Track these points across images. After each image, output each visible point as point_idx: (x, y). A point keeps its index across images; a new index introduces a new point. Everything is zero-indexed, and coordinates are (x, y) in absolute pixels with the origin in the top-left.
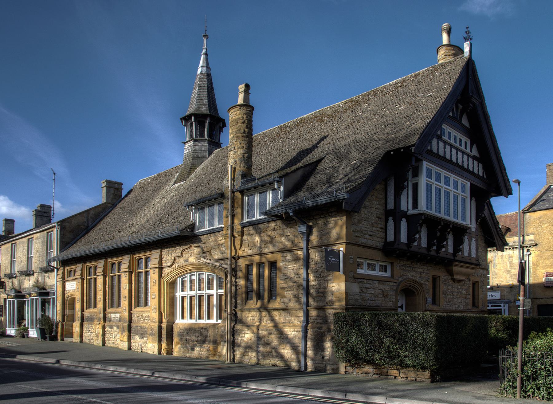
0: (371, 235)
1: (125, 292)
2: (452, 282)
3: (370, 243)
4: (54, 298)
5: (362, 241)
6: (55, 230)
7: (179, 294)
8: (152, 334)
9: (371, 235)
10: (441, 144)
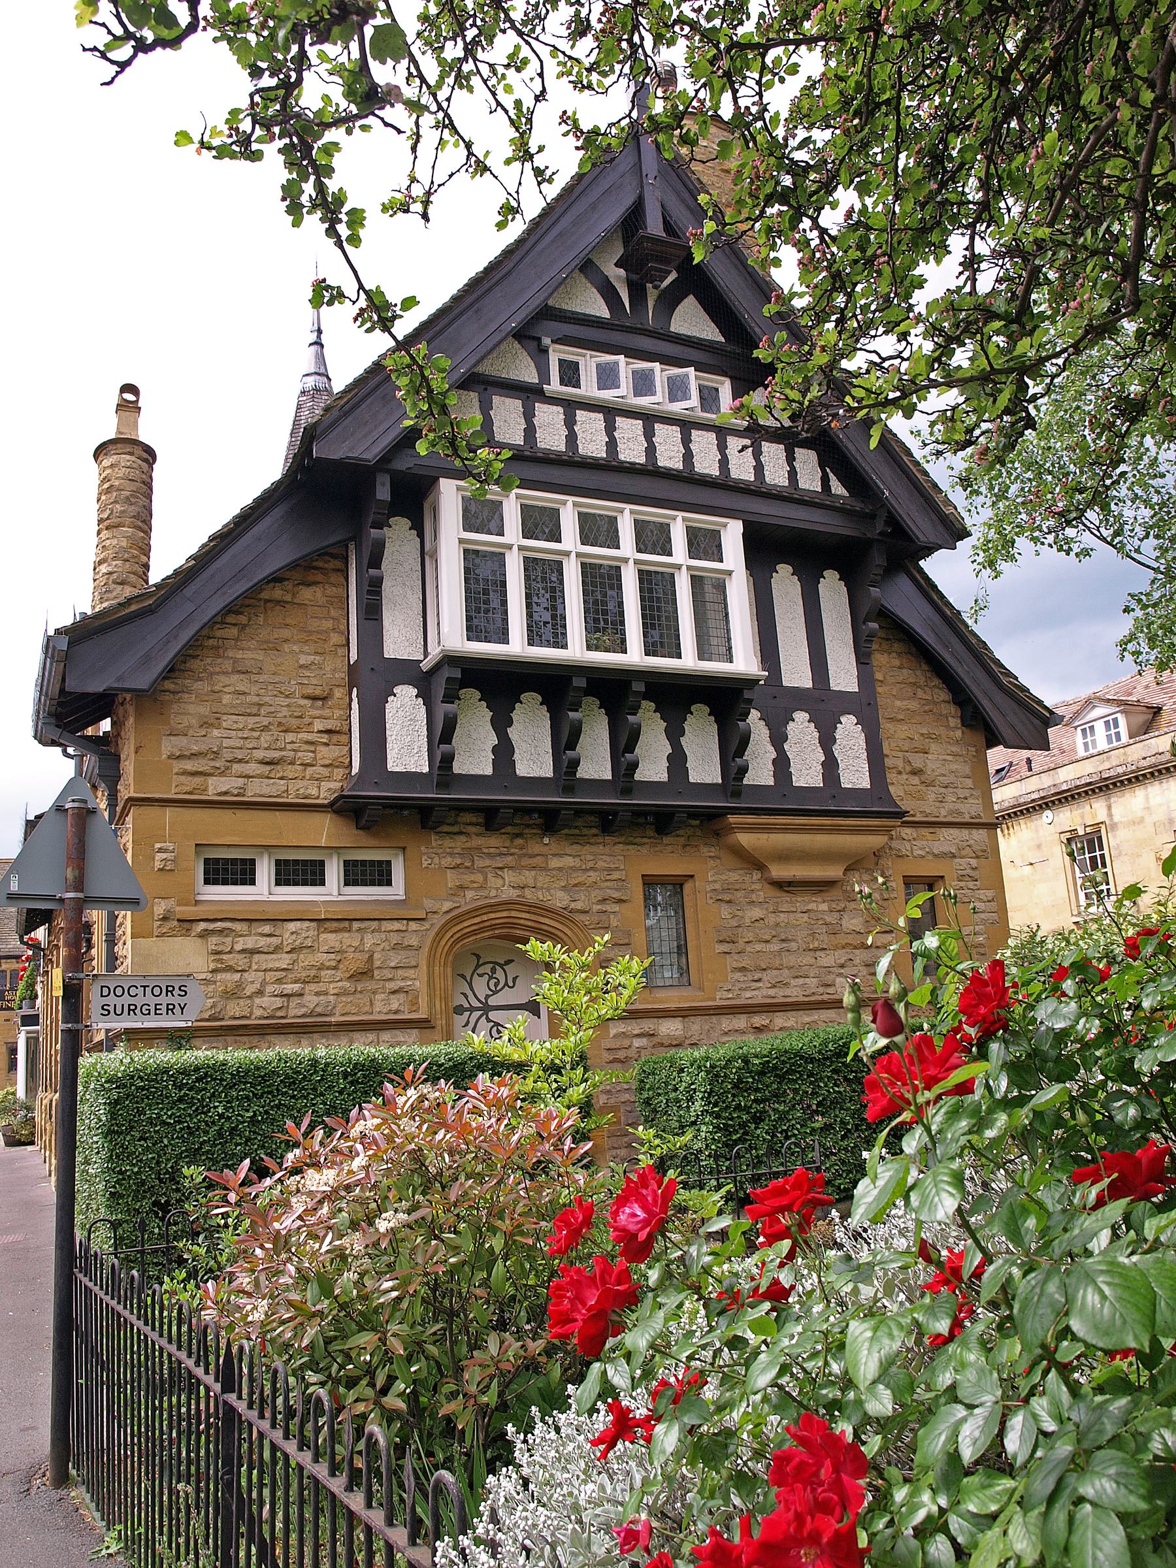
2: (762, 893)
5: (215, 787)
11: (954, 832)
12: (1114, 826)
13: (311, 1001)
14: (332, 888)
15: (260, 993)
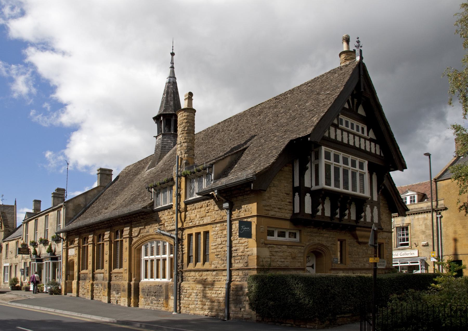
0: (279, 209)
1: (106, 257)
2: (356, 244)
3: (278, 215)
4: (60, 262)
5: (271, 213)
6: (62, 209)
7: (144, 258)
8: (124, 291)
9: (279, 209)
10: (339, 132)
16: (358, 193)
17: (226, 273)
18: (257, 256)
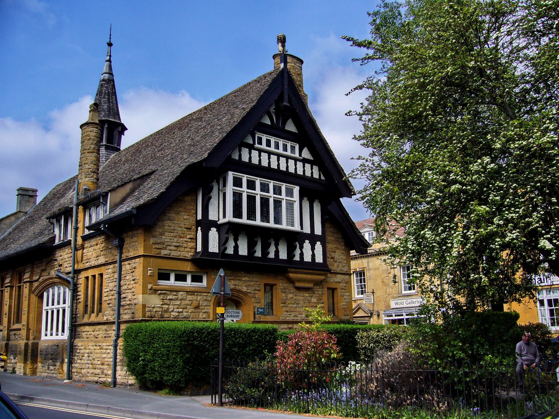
2: (293, 290)
5: (164, 252)
8: (20, 354)
11: (341, 276)
12: (369, 269)
13: (185, 314)
14: (189, 283)
15: (173, 311)
16: (284, 226)
17: (114, 327)
18: (143, 305)
